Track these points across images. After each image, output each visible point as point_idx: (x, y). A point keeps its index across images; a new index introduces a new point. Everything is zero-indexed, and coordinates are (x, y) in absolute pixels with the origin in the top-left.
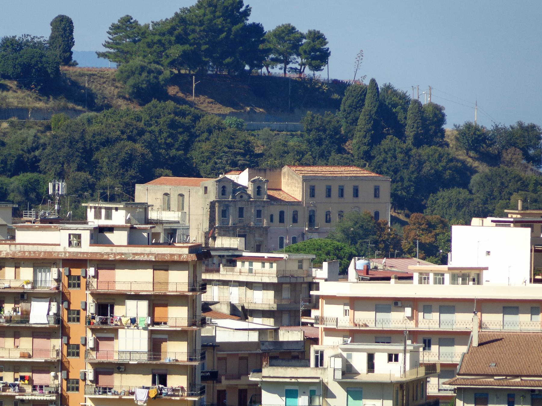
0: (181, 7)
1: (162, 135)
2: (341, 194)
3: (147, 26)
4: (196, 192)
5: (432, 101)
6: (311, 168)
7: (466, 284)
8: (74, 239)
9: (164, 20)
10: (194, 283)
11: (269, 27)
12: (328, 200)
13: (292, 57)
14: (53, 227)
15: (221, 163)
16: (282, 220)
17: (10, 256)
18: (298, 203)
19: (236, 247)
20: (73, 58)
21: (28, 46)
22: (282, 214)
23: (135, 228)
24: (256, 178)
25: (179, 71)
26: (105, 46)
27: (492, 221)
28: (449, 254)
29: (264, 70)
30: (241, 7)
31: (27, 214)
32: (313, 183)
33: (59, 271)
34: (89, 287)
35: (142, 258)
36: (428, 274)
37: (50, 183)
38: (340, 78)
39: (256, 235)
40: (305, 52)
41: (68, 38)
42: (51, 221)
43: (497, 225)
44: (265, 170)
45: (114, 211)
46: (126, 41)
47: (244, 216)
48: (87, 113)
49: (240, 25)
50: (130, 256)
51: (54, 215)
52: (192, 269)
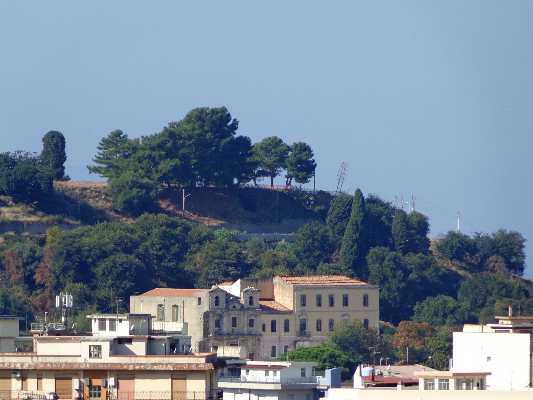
0: (170, 122)
1: (154, 247)
2: (346, 302)
3: (137, 141)
4: (190, 303)
5: (416, 210)
6: (302, 278)
7: (470, 389)
8: (95, 350)
9: (154, 135)
10: (211, 392)
11: (256, 140)
12: (319, 309)
13: (278, 169)
14: (73, 339)
15: (213, 273)
16: (274, 329)
17: (32, 368)
18: (290, 312)
19: (237, 356)
20: (65, 174)
21: (22, 162)
22: (274, 323)
23: (154, 339)
24: (248, 288)
25: (169, 185)
26: (95, 161)
27: (492, 328)
28: (450, 360)
29: (252, 182)
30: (229, 121)
31: (35, 327)
32: (304, 292)
33: (80, 382)
34: (109, 397)
35: (160, 368)
36: (433, 380)
37: (57, 296)
38: (325, 189)
39: (249, 344)
40: (292, 164)
41: (60, 154)
42: (58, 333)
43: (496, 332)
44: (257, 281)
45: (118, 322)
46: (116, 156)
47: (238, 326)
48: (80, 228)
49: (228, 139)
50: (149, 366)
51: (62, 327)
52: (208, 377)
